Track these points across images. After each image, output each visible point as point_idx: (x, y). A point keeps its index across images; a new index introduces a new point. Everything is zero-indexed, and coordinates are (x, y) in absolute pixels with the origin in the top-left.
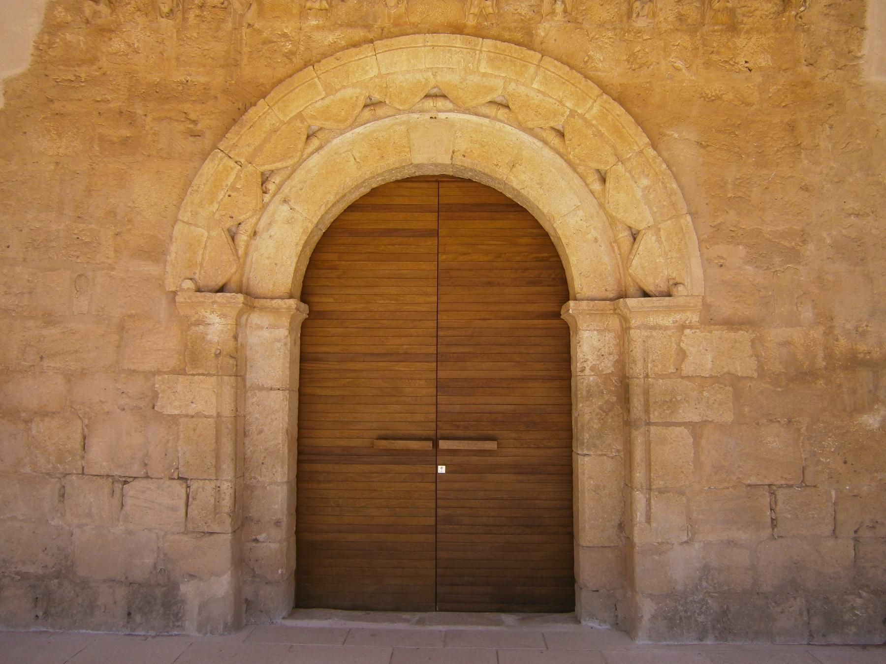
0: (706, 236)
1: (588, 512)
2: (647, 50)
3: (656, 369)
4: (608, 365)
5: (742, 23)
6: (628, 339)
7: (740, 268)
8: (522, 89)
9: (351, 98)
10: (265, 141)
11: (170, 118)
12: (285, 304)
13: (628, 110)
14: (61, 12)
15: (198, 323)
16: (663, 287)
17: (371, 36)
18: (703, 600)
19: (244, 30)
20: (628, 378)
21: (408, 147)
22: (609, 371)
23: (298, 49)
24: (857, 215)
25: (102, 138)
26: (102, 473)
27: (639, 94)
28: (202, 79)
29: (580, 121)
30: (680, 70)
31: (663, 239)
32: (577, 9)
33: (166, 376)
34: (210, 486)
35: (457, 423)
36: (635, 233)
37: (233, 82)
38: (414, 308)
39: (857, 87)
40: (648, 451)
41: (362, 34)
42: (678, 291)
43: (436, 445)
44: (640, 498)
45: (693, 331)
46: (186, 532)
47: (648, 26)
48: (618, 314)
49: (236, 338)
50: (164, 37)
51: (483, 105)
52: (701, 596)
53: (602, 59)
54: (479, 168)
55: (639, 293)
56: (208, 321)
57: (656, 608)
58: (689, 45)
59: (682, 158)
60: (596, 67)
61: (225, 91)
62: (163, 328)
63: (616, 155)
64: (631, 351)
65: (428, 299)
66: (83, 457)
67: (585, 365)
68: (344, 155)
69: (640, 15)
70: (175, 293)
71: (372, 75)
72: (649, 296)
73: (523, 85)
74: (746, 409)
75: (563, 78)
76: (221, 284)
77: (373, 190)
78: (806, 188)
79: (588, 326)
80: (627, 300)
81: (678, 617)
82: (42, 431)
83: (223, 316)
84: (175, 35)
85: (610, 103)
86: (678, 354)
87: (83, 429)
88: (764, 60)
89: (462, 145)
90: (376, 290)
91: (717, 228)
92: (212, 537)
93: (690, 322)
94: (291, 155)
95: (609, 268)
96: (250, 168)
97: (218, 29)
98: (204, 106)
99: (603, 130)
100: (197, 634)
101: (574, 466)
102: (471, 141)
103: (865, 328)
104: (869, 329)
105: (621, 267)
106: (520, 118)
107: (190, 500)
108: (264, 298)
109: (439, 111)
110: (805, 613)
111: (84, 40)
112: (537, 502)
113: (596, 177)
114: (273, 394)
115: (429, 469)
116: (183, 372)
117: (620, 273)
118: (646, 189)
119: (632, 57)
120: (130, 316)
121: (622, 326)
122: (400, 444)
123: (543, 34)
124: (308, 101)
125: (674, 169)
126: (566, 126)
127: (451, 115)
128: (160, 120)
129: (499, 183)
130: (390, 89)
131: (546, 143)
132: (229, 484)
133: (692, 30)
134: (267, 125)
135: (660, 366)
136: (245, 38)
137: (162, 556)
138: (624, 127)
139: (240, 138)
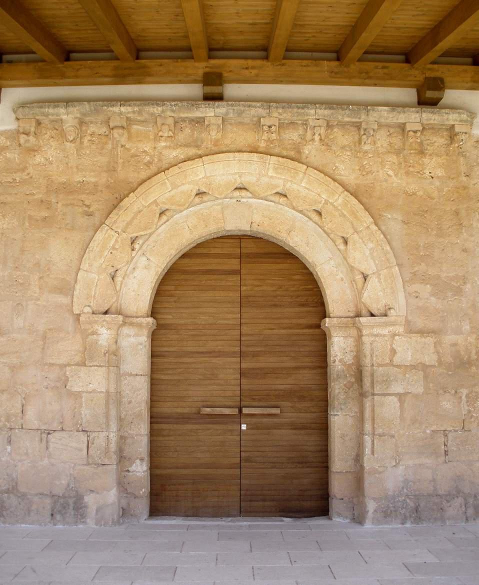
0: (408, 279)
2: (371, 163)
3: (378, 361)
4: (349, 359)
5: (427, 150)
7: (427, 299)
8: (295, 186)
9: (188, 191)
10: (133, 218)
11: (73, 204)
12: (146, 320)
14: (3, 140)
15: (93, 333)
16: (382, 311)
17: (200, 152)
18: (404, 500)
19: (119, 149)
20: (361, 366)
22: (350, 362)
23: (153, 160)
25: (30, 217)
26: (34, 428)
27: (367, 191)
28: (93, 180)
29: (331, 207)
30: (391, 176)
31: (382, 281)
32: (328, 137)
33: (73, 367)
34: (103, 435)
35: (254, 397)
37: (113, 181)
38: (226, 322)
40: (373, 411)
41: (194, 151)
42: (391, 313)
43: (240, 411)
44: (368, 439)
45: (400, 337)
46: (88, 464)
48: (356, 327)
49: (116, 342)
50: (68, 153)
51: (271, 195)
52: (403, 498)
55: (368, 314)
56: (99, 332)
57: (377, 505)
58: (395, 161)
59: (393, 230)
61: (108, 187)
62: (71, 337)
65: (234, 316)
66: (22, 418)
68: (182, 224)
70: (79, 315)
71: (201, 177)
73: (295, 183)
74: (431, 385)
75: (320, 181)
76: (106, 309)
77: (198, 244)
78: (465, 250)
79: (337, 334)
80: (361, 319)
81: (389, 511)
83: (109, 329)
84: (75, 152)
86: (391, 351)
87: (22, 400)
88: (440, 172)
89: (257, 218)
90: (201, 310)
91: (414, 274)
92: (104, 467)
94: (150, 227)
95: (350, 297)
96: (124, 235)
97: (103, 148)
98: (94, 196)
99: (345, 213)
100: (95, 526)
101: (329, 423)
102: (263, 216)
106: (294, 204)
107: (90, 444)
108: (131, 317)
109: (242, 198)
110: (464, 507)
112: (304, 447)
114: (138, 378)
115: (236, 427)
116: (83, 364)
118: (372, 249)
119: (361, 169)
120: (50, 330)
122: (218, 411)
123: (307, 152)
125: (388, 237)
127: (251, 200)
128: (67, 205)
132: (114, 434)
133: (398, 152)
134: (135, 208)
137: (72, 479)
138: (358, 212)
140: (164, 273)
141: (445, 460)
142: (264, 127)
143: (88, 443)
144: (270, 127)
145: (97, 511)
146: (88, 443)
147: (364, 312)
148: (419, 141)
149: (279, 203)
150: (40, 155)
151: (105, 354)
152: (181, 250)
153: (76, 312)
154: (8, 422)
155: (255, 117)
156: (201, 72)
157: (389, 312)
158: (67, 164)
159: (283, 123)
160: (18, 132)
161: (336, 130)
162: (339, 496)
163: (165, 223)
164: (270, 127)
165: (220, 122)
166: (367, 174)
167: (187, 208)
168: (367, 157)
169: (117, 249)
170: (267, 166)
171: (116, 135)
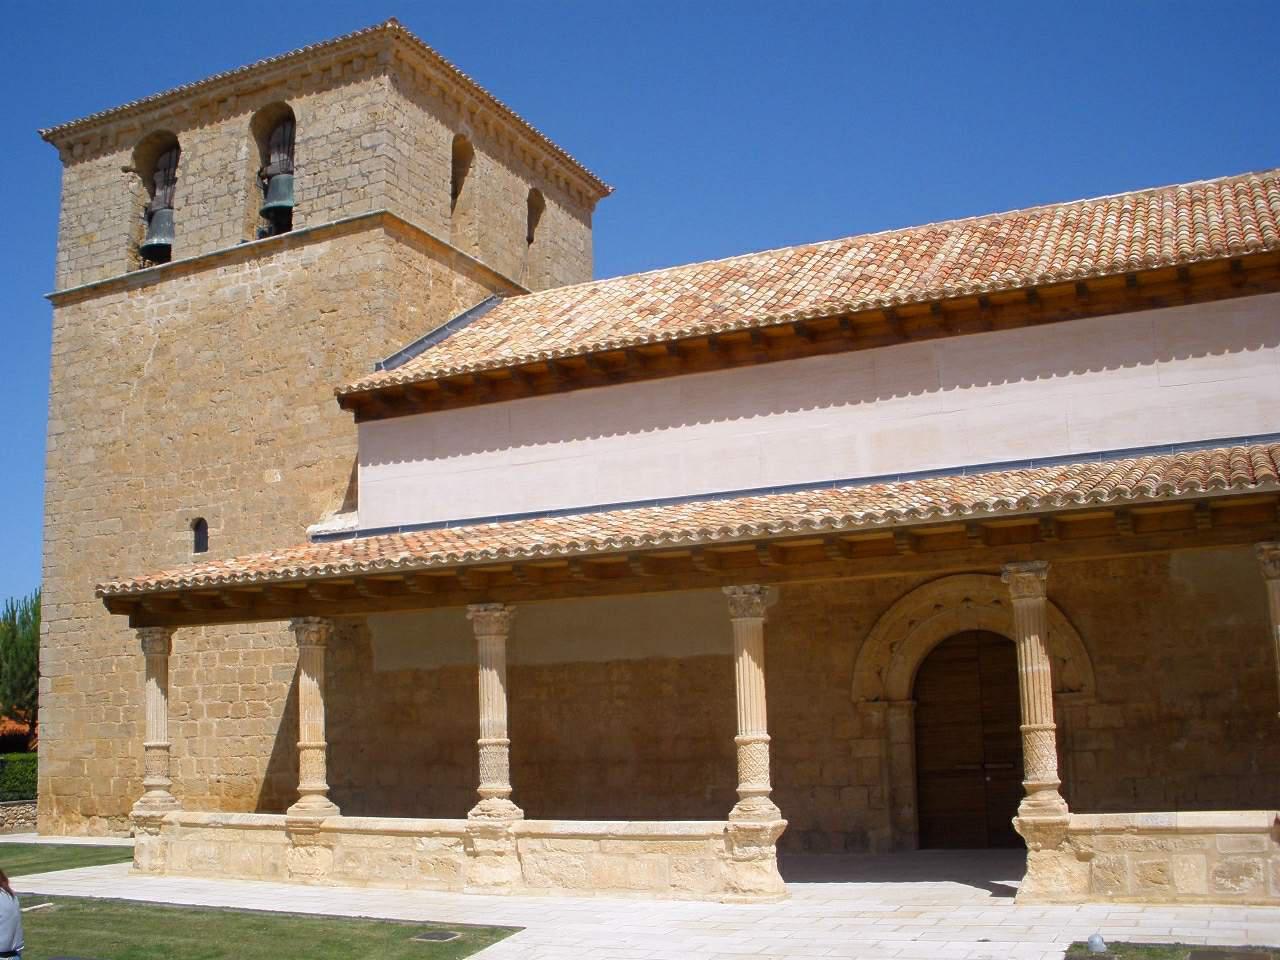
107: (550, 521)
116: (862, 738)
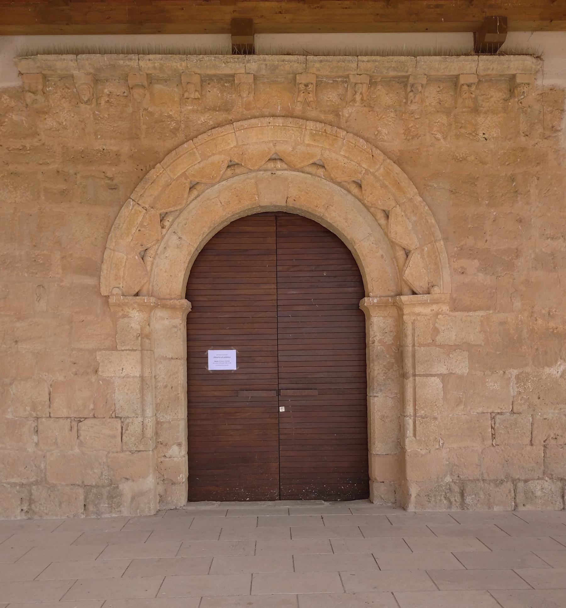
1: (377, 432)
2: (417, 126)
3: (420, 341)
5: (481, 107)
6: (402, 322)
8: (334, 155)
9: (219, 162)
13: (403, 170)
14: (7, 99)
15: (124, 316)
21: (257, 195)
24: (552, 238)
27: (412, 157)
28: (114, 148)
29: (372, 177)
30: (439, 140)
31: (425, 256)
33: (104, 352)
36: (408, 252)
39: (557, 151)
45: (444, 316)
47: (418, 109)
48: (396, 306)
51: (308, 166)
53: (387, 132)
54: (304, 209)
55: (410, 292)
56: (130, 315)
60: (383, 139)
61: (131, 157)
63: (395, 200)
64: (404, 329)
67: (375, 339)
68: (213, 200)
69: (413, 101)
70: (107, 297)
71: (232, 146)
72: (416, 294)
73: (334, 152)
76: (137, 291)
78: (520, 221)
79: (377, 314)
80: (402, 297)
82: (20, 390)
84: (92, 116)
85: (391, 165)
88: (495, 133)
92: (140, 453)
93: (442, 311)
95: (391, 275)
96: (153, 211)
98: (117, 167)
99: (387, 183)
101: (368, 405)
103: (554, 313)
104: (557, 313)
105: (398, 274)
107: (124, 431)
109: (277, 170)
111: (26, 120)
113: (382, 215)
116: (115, 348)
117: (368, 61)
121: (398, 313)
124: (190, 165)
126: (363, 181)
129: (318, 218)
130: (245, 156)
131: (349, 191)
133: (448, 113)
134: (163, 181)
135: (422, 339)
136: (142, 118)
139: (145, 191)
140: (197, 253)
141: (492, 444)
142: (300, 86)
143: (122, 429)
144: (306, 85)
145: (133, 499)
146: (122, 429)
147: (406, 290)
148: (473, 96)
149: (316, 175)
150: (51, 119)
151: (137, 338)
152: (215, 228)
153: (104, 292)
154: (34, 412)
155: (289, 74)
156: (228, 18)
157: (432, 290)
158: (83, 129)
159: (321, 81)
160: (23, 90)
161: (379, 87)
162: (379, 479)
163: (196, 198)
164: (306, 85)
165: (252, 80)
166: (412, 139)
167: (219, 182)
168: (413, 119)
169: (144, 227)
170: (304, 132)
171: (136, 96)
